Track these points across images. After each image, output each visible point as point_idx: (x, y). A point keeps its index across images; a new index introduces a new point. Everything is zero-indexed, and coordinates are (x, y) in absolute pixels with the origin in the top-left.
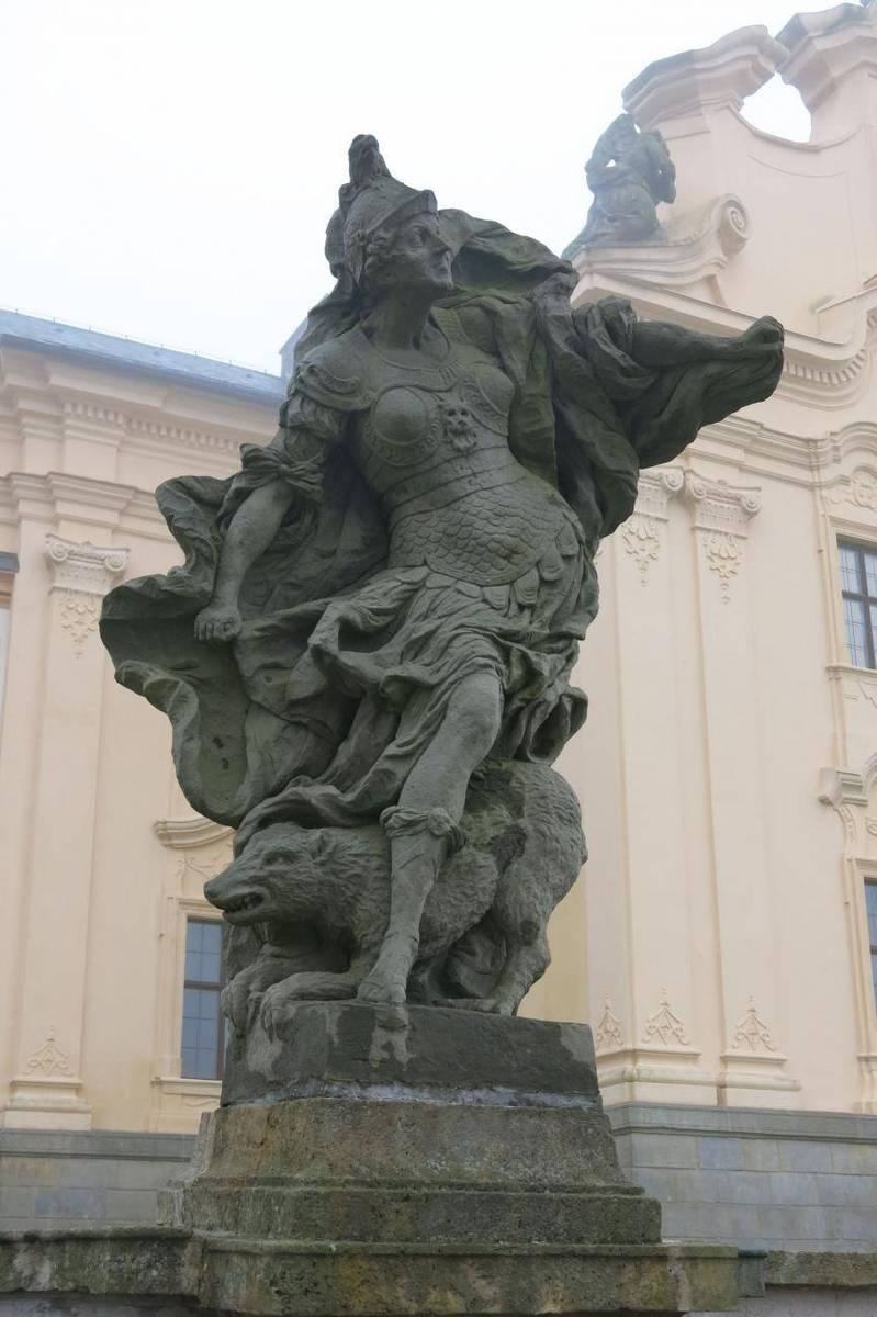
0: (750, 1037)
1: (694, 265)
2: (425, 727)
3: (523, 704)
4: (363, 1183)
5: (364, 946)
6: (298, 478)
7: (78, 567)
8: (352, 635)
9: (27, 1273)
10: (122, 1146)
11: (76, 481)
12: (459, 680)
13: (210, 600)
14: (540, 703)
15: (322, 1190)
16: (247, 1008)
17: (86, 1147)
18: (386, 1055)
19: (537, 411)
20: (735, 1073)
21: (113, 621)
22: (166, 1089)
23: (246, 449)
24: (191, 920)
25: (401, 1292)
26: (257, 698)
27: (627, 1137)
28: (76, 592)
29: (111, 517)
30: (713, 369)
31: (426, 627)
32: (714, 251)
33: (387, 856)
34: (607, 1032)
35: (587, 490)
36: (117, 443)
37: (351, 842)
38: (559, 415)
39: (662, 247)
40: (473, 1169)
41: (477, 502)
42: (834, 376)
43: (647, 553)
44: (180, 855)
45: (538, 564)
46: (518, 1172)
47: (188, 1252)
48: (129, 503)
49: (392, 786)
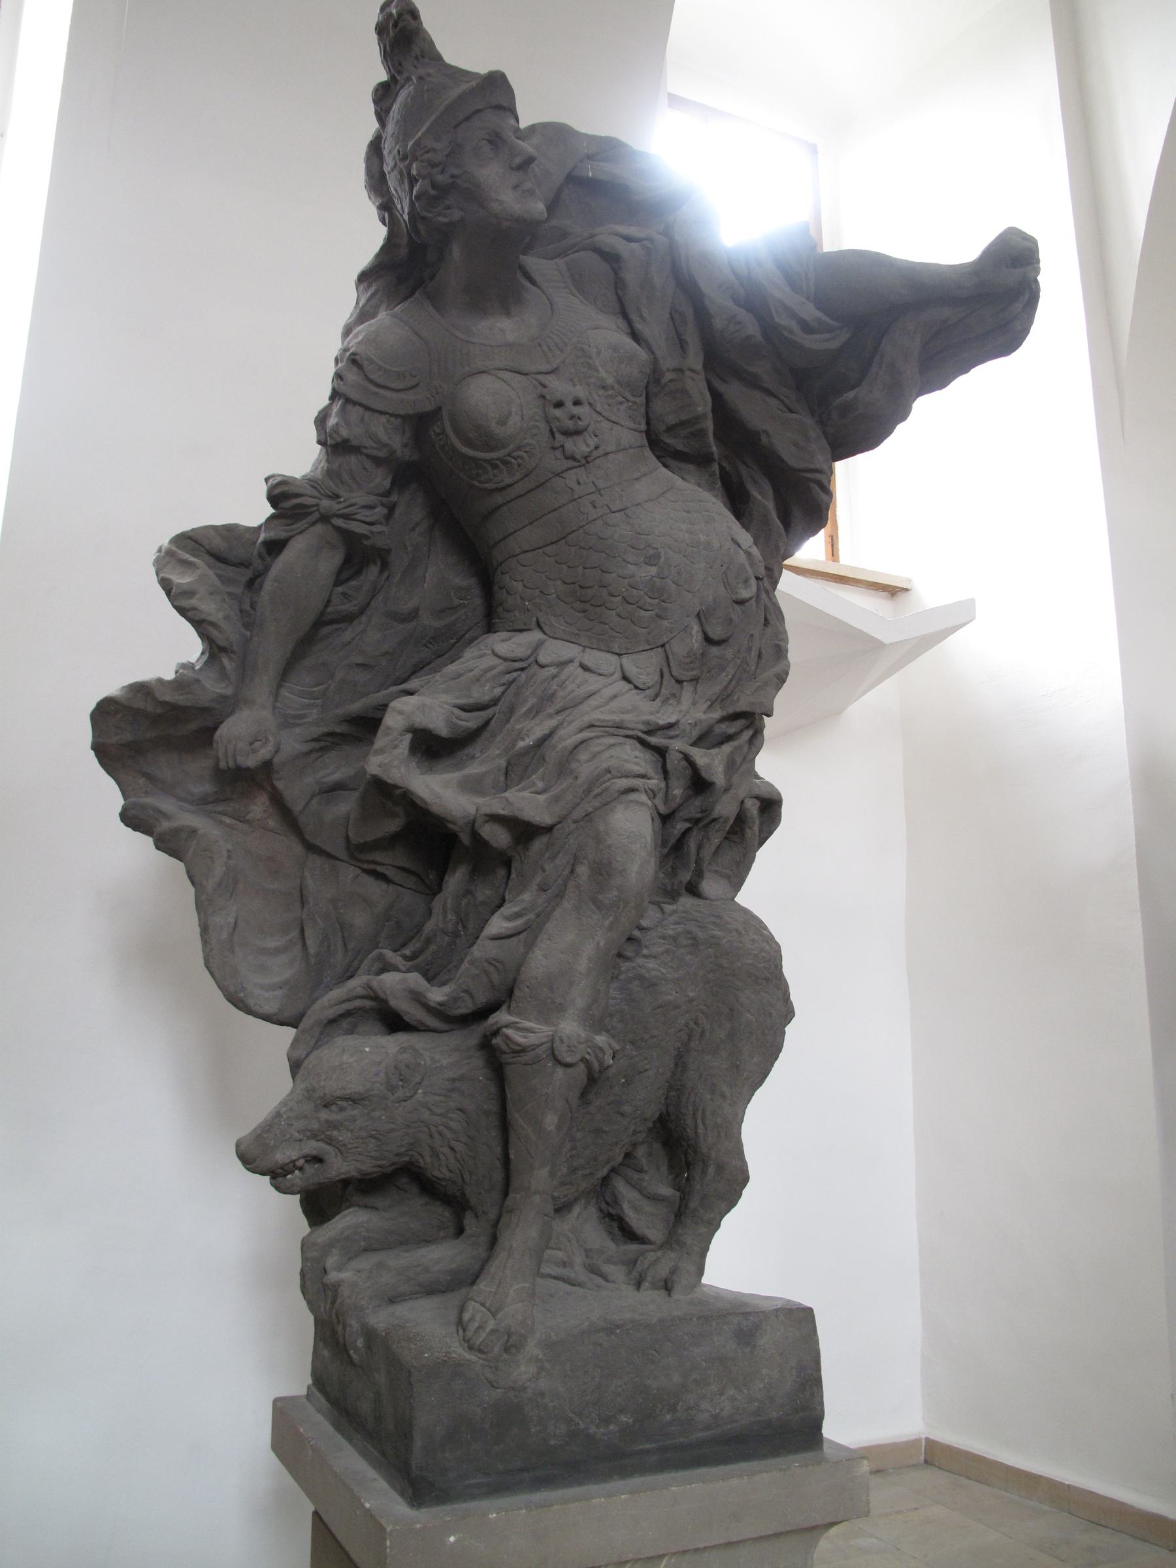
3: (687, 825)
8: (431, 747)
13: (226, 707)
14: (715, 820)
23: (271, 482)
31: (538, 729)
35: (763, 497)
38: (716, 396)
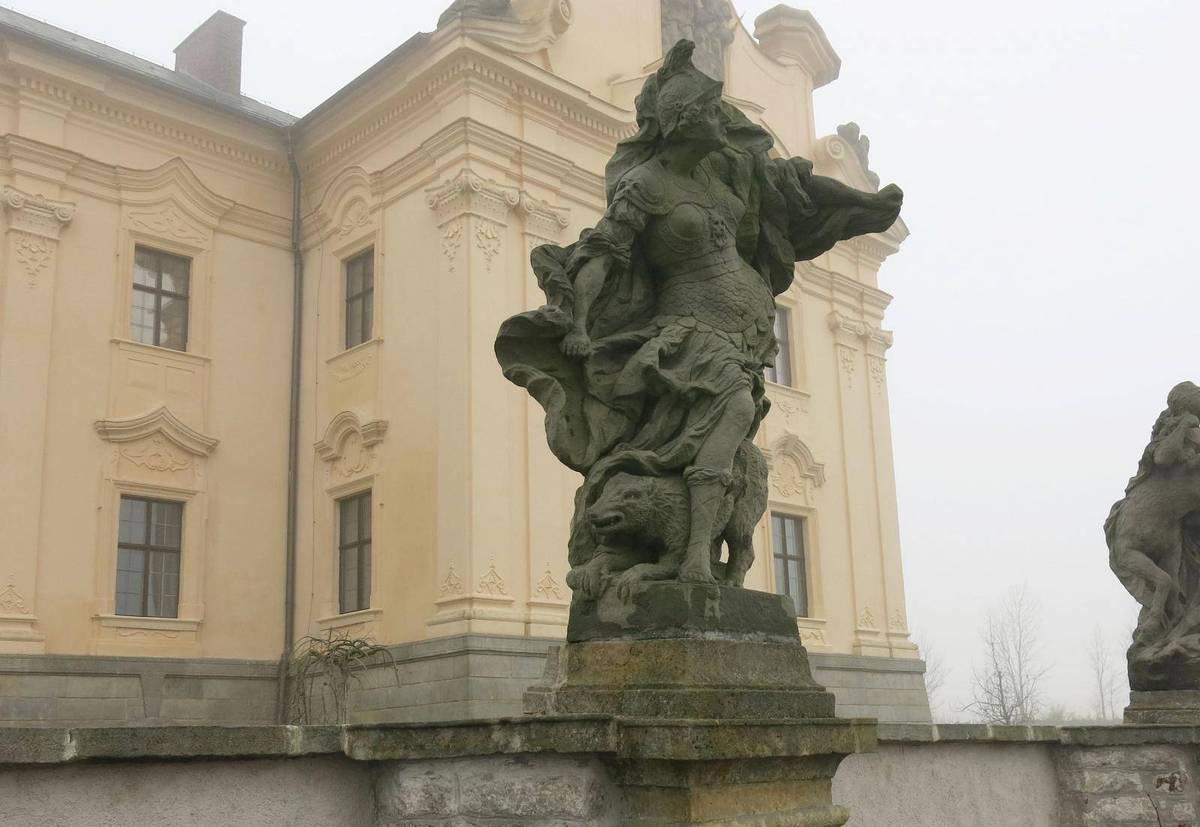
0: (490, 585)
1: (536, 40)
2: (712, 419)
4: (711, 686)
5: (670, 548)
6: (620, 254)
7: (32, 214)
9: (501, 743)
10: (70, 665)
11: (33, 144)
12: (733, 393)
15: (698, 691)
16: (600, 584)
17: (41, 667)
18: (711, 614)
19: (751, 224)
20: (537, 614)
21: (509, 337)
22: (104, 623)
24: (124, 496)
25: (746, 746)
26: (593, 392)
27: (465, 657)
28: (30, 234)
29: (61, 177)
30: (856, 211)
32: (547, 30)
33: (688, 498)
34: (451, 585)
36: (64, 116)
37: (666, 486)
39: (511, 22)
40: (753, 677)
41: (728, 280)
42: (616, 132)
43: (491, 248)
44: (115, 447)
45: (756, 321)
46: (771, 680)
47: (611, 728)
48: (75, 166)
49: (691, 455)
